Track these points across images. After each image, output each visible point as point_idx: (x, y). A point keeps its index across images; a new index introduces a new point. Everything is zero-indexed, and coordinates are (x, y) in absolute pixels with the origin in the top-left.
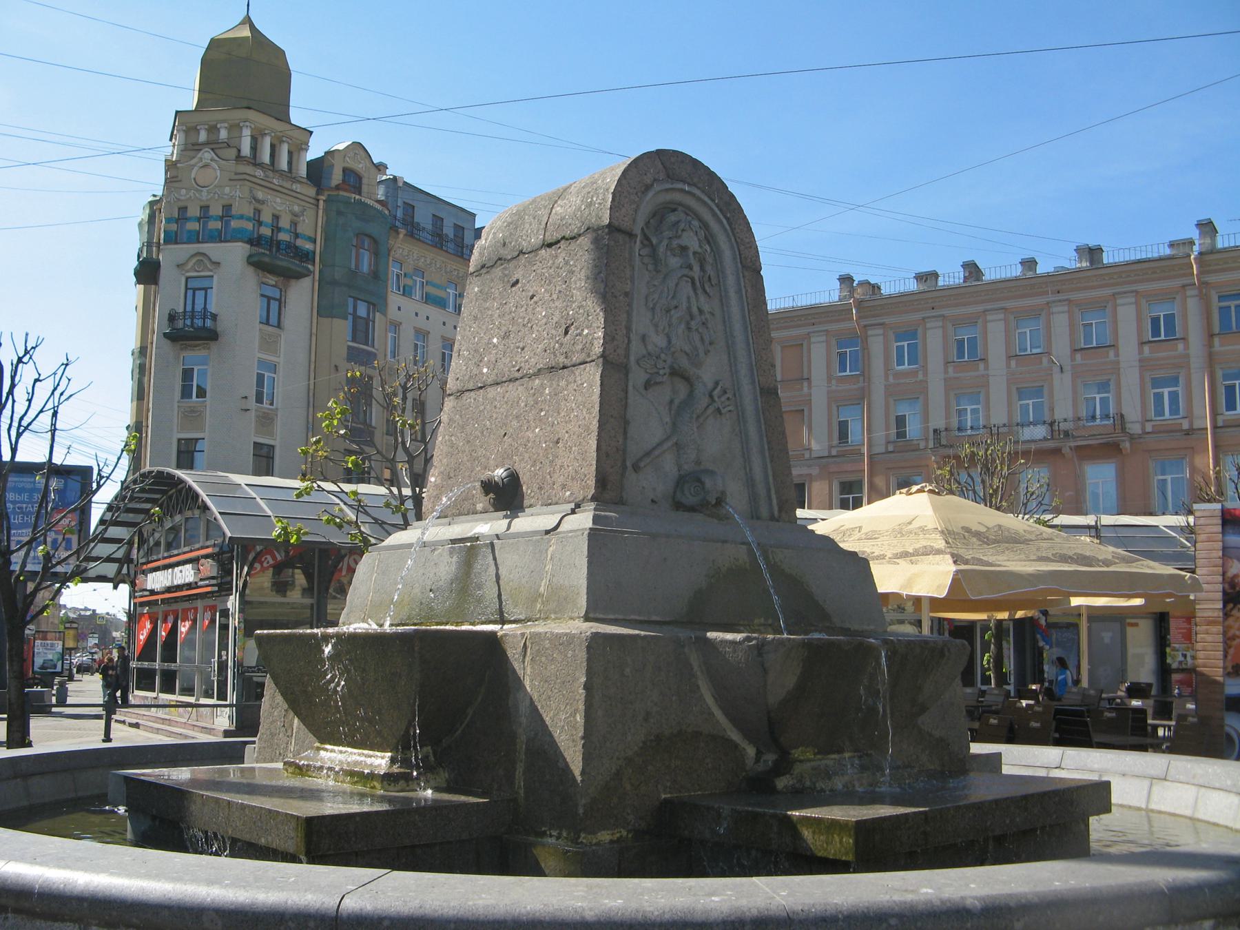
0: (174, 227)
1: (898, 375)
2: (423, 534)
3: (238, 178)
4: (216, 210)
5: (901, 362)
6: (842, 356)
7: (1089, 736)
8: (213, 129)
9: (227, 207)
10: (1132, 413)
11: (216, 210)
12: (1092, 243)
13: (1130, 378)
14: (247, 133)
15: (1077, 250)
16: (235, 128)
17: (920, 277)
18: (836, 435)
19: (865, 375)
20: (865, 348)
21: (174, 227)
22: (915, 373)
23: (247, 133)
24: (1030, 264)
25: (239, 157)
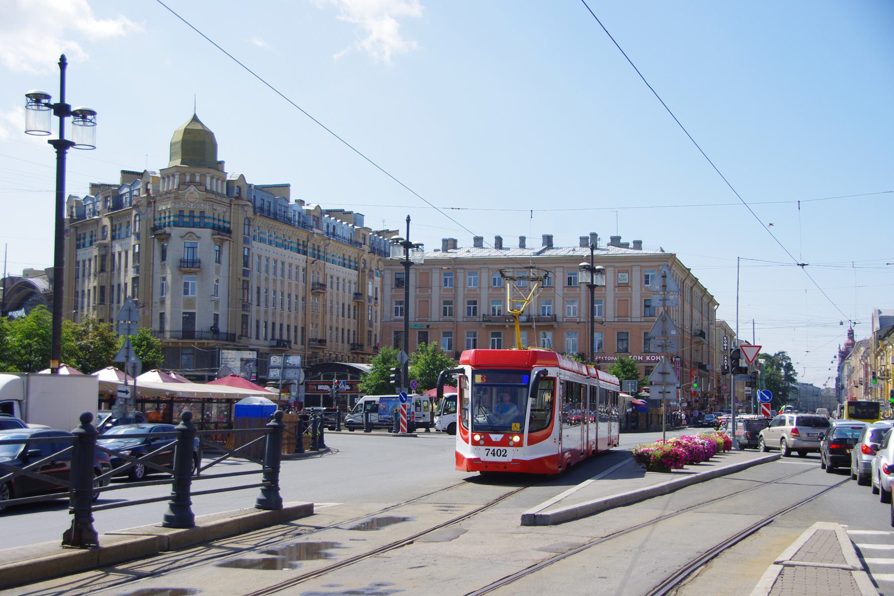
0: (177, 219)
1: (469, 290)
3: (207, 200)
4: (197, 214)
5: (470, 285)
6: (446, 280)
8: (193, 175)
9: (202, 212)
10: (559, 314)
11: (197, 214)
12: (549, 234)
13: (559, 301)
14: (208, 179)
15: (544, 236)
16: (203, 176)
17: (584, 242)
18: (442, 313)
19: (456, 287)
20: (456, 278)
21: (177, 219)
22: (476, 290)
23: (208, 179)
24: (450, 244)
25: (206, 191)
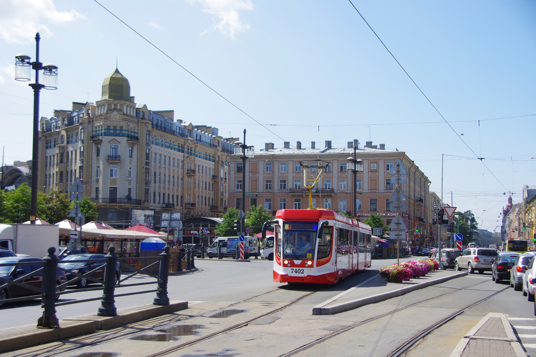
0: (106, 131)
1: (281, 174)
2: (512, 341)
3: (124, 120)
4: (118, 128)
5: (282, 170)
6: (267, 168)
7: (334, 215)
8: (116, 105)
9: (121, 127)
10: (335, 188)
11: (118, 128)
12: (329, 140)
13: (335, 180)
14: (125, 107)
15: (326, 142)
16: (122, 105)
18: (265, 188)
19: (273, 172)
20: (273, 166)
21: (106, 131)
22: (285, 174)
23: (125, 107)
25: (124, 114)
